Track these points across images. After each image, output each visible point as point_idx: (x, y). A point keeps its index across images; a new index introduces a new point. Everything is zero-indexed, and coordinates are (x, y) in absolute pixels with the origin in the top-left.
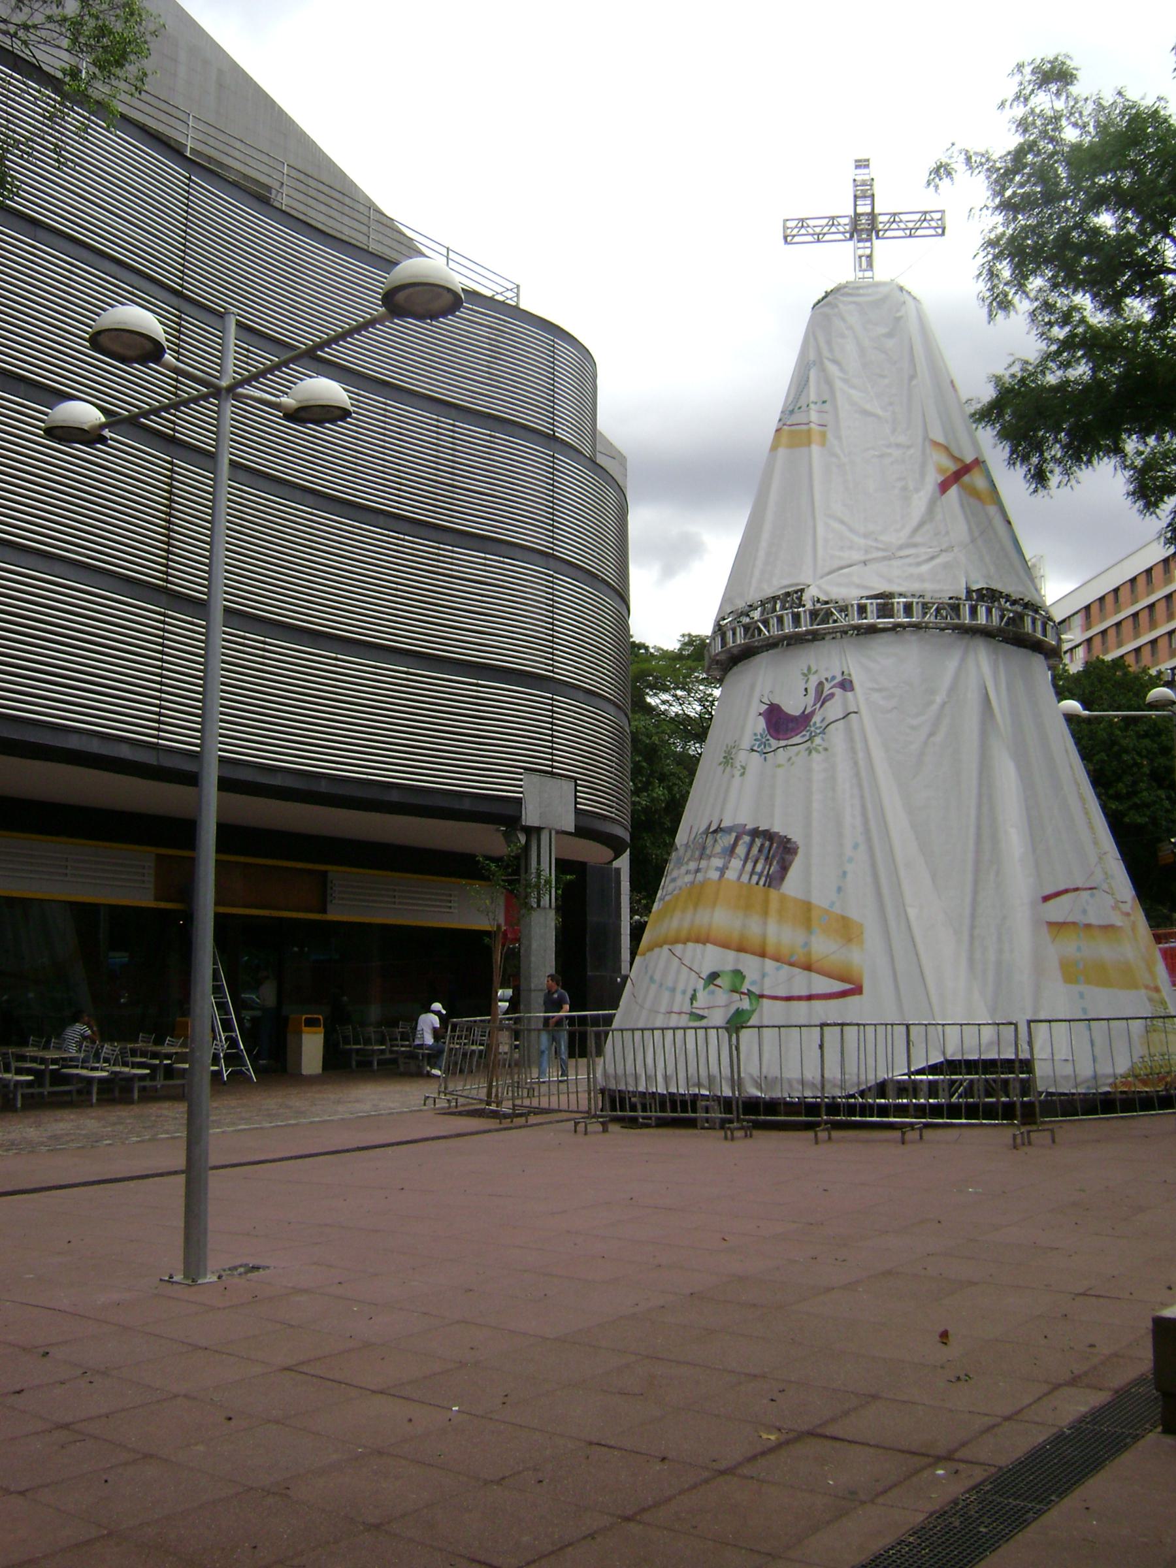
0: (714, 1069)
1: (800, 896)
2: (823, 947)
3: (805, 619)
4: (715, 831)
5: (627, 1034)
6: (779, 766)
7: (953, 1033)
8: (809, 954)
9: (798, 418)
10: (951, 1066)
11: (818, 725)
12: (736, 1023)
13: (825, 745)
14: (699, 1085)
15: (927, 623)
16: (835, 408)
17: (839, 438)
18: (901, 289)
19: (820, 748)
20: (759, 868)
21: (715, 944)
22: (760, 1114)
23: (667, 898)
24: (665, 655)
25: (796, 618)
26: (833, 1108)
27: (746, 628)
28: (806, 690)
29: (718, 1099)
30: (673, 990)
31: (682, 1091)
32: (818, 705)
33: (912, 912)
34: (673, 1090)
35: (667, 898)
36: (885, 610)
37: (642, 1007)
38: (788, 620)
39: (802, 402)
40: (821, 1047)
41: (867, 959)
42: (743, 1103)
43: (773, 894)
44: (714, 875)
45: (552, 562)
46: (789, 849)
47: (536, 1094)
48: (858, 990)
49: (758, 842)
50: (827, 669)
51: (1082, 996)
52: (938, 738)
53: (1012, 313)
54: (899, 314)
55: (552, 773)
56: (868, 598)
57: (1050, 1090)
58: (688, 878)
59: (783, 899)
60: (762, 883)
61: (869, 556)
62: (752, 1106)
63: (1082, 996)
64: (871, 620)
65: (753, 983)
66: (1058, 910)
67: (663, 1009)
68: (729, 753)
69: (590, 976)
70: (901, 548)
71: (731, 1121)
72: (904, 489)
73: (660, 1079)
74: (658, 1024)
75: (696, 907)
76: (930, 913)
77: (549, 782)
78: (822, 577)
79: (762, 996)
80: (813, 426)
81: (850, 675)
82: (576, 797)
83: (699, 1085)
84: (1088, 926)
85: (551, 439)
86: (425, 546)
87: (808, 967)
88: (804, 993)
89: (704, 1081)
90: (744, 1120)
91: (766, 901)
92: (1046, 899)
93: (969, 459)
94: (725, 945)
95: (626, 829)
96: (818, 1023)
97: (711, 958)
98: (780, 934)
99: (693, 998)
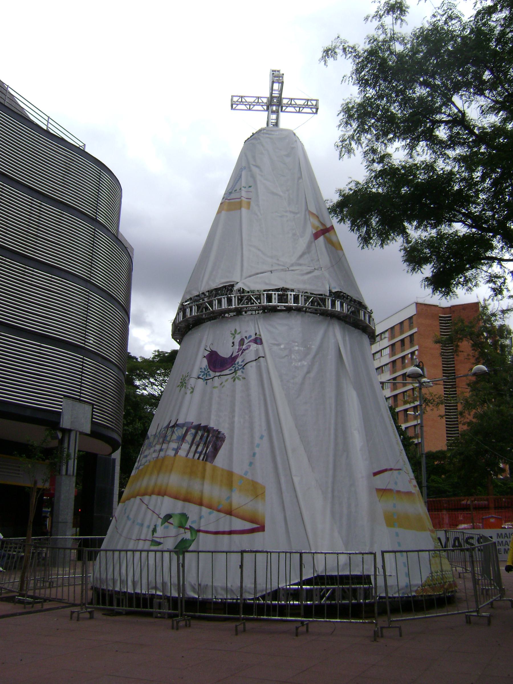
0: (167, 579)
1: (226, 467)
2: (239, 500)
3: (235, 301)
4: (173, 426)
5: (110, 554)
6: (214, 387)
7: (320, 558)
8: (231, 504)
9: (233, 196)
10: (319, 580)
11: (240, 364)
12: (182, 548)
13: (244, 376)
14: (156, 588)
15: (306, 308)
16: (256, 189)
17: (258, 205)
18: (295, 134)
19: (240, 377)
20: (200, 449)
21: (170, 496)
22: (193, 609)
23: (141, 467)
24: (145, 361)
25: (230, 301)
26: (248, 608)
27: (199, 307)
28: (233, 343)
29: (168, 598)
30: (142, 525)
31: (144, 592)
32: (240, 352)
33: (296, 480)
34: (138, 591)
35: (141, 467)
36: (282, 298)
37: (121, 535)
38: (224, 302)
39: (237, 187)
40: (241, 567)
41: (269, 509)
42: (186, 601)
43: (208, 464)
44: (171, 453)
45: (89, 285)
46: (220, 438)
47: (55, 585)
48: (262, 529)
49: (200, 433)
50: (246, 332)
51: (397, 535)
52: (312, 375)
53: (352, 155)
54: (293, 146)
55: (79, 400)
56: (273, 290)
57: (381, 595)
58: (155, 455)
59: (215, 468)
60: (201, 458)
61: (274, 268)
62: (192, 605)
63: (397, 535)
64: (275, 302)
65: (193, 522)
66: (381, 481)
67: (134, 537)
68: (184, 380)
69: (93, 516)
70: (292, 265)
71: (176, 616)
72: (294, 235)
73: (130, 583)
74: (130, 547)
75: (158, 473)
76: (306, 478)
77: (78, 404)
78: (246, 278)
79: (199, 531)
80: (243, 198)
81: (260, 335)
82: (93, 414)
83: (156, 588)
84: (398, 492)
85: (94, 221)
86: (18, 265)
87: (229, 513)
88: (227, 529)
89: (159, 586)
90: (185, 615)
91: (204, 470)
92: (375, 474)
93: (328, 226)
94: (176, 497)
95: (120, 435)
96: (239, 550)
97: (167, 505)
98: (211, 491)
99: (154, 530)
